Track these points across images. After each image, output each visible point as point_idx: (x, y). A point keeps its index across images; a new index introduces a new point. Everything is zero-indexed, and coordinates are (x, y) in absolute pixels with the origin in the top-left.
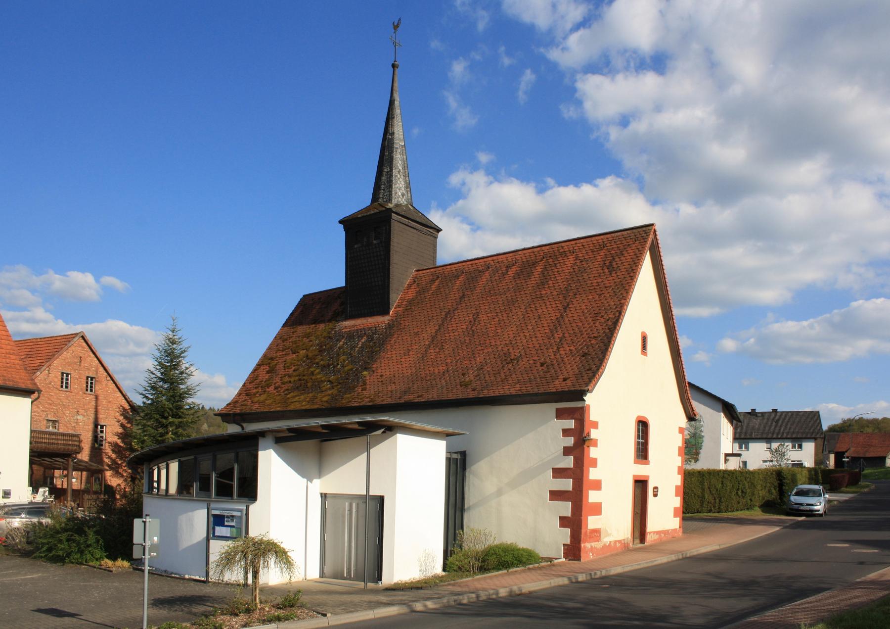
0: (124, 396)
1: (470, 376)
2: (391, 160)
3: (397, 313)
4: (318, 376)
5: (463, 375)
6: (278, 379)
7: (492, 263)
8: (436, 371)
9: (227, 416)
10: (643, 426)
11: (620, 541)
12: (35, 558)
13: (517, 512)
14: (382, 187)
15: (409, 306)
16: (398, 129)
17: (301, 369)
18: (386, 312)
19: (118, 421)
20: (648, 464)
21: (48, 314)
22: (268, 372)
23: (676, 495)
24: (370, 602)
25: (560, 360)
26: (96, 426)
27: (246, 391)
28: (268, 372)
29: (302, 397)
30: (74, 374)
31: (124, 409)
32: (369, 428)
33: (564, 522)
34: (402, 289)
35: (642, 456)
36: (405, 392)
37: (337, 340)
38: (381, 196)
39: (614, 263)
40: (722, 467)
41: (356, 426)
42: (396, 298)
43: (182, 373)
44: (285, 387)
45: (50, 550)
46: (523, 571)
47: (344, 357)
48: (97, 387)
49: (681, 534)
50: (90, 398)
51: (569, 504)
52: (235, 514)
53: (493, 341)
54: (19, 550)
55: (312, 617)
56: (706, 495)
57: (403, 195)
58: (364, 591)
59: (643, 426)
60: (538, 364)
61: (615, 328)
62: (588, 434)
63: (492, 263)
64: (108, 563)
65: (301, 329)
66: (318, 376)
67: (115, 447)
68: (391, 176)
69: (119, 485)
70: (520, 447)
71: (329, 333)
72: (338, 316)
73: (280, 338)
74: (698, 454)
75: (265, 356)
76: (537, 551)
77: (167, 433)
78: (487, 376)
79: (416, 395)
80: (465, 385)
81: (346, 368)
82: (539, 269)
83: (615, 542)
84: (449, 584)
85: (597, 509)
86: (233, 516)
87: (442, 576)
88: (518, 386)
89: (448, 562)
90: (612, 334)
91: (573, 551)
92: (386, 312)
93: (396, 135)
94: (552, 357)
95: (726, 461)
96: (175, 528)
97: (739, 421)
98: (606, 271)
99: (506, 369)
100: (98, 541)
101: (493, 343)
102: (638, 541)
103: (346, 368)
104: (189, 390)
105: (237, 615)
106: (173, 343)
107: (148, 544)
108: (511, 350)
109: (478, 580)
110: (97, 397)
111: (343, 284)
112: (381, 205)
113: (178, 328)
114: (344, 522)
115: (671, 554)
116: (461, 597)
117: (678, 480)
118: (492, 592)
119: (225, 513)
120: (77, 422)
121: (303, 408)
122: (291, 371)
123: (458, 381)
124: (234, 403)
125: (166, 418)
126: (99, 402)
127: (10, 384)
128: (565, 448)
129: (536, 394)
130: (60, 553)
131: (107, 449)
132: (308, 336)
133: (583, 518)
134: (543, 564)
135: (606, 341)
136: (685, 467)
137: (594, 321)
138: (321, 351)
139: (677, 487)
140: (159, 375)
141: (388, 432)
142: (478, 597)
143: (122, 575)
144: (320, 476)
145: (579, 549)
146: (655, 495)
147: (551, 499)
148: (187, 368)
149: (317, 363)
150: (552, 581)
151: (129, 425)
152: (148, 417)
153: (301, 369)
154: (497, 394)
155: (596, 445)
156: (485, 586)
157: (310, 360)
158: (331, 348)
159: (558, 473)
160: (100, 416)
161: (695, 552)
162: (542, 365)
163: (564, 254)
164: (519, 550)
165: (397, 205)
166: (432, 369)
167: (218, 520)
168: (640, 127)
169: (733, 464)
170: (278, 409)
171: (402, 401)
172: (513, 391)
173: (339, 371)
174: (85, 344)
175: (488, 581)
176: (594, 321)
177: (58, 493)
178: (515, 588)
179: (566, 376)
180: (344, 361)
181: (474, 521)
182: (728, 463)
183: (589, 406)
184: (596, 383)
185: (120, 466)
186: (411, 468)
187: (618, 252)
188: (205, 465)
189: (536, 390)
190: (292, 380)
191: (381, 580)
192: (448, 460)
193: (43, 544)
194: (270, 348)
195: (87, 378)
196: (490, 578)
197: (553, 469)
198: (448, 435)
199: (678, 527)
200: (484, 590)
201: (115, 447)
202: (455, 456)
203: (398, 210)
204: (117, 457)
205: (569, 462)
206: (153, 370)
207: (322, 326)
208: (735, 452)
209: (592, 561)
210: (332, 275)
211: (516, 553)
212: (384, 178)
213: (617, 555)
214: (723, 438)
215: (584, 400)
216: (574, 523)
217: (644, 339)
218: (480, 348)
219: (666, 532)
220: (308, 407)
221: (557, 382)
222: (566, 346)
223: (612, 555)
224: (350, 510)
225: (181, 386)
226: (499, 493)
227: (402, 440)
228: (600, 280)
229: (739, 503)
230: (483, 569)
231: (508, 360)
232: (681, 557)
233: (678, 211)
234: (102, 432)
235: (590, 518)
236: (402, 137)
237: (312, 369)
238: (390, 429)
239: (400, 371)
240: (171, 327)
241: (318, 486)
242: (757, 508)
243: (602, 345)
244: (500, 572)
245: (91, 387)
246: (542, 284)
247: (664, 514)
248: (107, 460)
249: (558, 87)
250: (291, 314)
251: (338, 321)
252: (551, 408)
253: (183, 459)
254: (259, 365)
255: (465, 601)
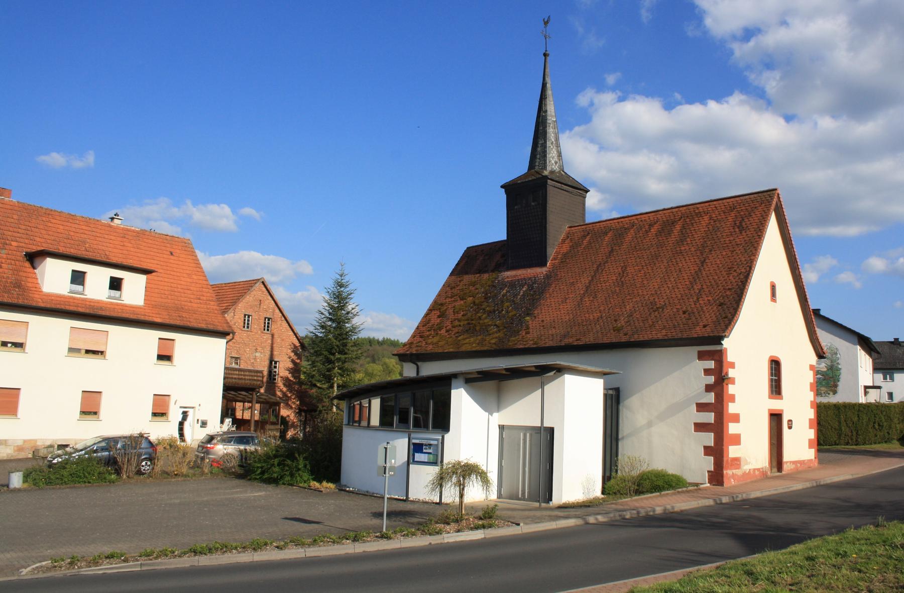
0: (295, 334)
1: (622, 322)
2: (545, 133)
3: (553, 265)
5: (616, 321)
6: (448, 323)
8: (591, 317)
10: (775, 365)
11: (758, 470)
13: (667, 442)
15: (565, 258)
16: (551, 108)
17: (469, 314)
19: (290, 358)
20: (782, 399)
21: (137, 225)
22: (439, 317)
23: (810, 428)
26: (271, 363)
27: (419, 333)
28: (439, 317)
30: (255, 316)
31: (295, 346)
32: (542, 370)
33: (708, 451)
34: (556, 243)
36: (565, 336)
40: (862, 400)
41: (533, 369)
43: (348, 313)
44: (455, 330)
45: (263, 473)
46: (674, 494)
47: (507, 304)
48: (273, 327)
49: (816, 464)
50: (267, 337)
51: (712, 435)
52: (432, 442)
54: (233, 473)
56: (839, 427)
57: (556, 163)
59: (775, 365)
61: (747, 281)
62: (727, 374)
63: (636, 221)
64: (316, 484)
65: (467, 278)
68: (545, 147)
70: (668, 385)
71: (493, 282)
72: (499, 268)
74: (836, 386)
75: (435, 302)
77: (334, 368)
79: (575, 339)
80: (617, 330)
82: (678, 227)
83: (754, 470)
91: (717, 477)
93: (549, 113)
95: (866, 393)
96: (377, 453)
97: (878, 353)
100: (305, 466)
101: (641, 293)
102: (775, 470)
105: (448, 524)
107: (388, 465)
110: (273, 336)
112: (537, 173)
113: (346, 272)
117: (811, 414)
119: (424, 442)
121: (474, 349)
122: (460, 316)
123: (611, 326)
124: (410, 344)
125: (334, 354)
127: (211, 327)
129: (681, 339)
130: (275, 475)
131: (280, 383)
132: (473, 284)
133: (724, 447)
134: (690, 488)
135: (739, 292)
139: (810, 420)
140: (328, 315)
142: (638, 513)
143: (330, 494)
145: (722, 476)
146: (790, 428)
151: (298, 361)
152: (317, 353)
153: (469, 314)
154: (646, 338)
155: (733, 383)
156: (642, 505)
157: (477, 306)
159: (701, 407)
160: (275, 353)
161: (828, 481)
162: (684, 313)
163: (699, 215)
164: (669, 475)
165: (552, 172)
166: (587, 315)
167: (417, 448)
168: (775, 38)
169: (873, 397)
170: (451, 350)
173: (504, 316)
177: (236, 421)
178: (669, 507)
179: (706, 323)
181: (627, 450)
182: (868, 395)
183: (726, 349)
185: (289, 398)
186: (576, 402)
188: (405, 400)
190: (462, 324)
192: (605, 396)
194: (439, 295)
197: (697, 404)
199: (813, 457)
202: (611, 392)
203: (553, 177)
205: (710, 398)
206: (323, 311)
207: (486, 276)
208: (876, 384)
209: (734, 486)
210: (494, 229)
212: (539, 149)
213: (755, 482)
216: (716, 451)
217: (773, 287)
219: (802, 462)
220: (478, 348)
221: (698, 328)
222: (704, 296)
224: (525, 440)
225: (347, 325)
226: (650, 424)
227: (570, 380)
230: (638, 492)
233: (816, 124)
234: (275, 367)
235: (731, 448)
238: (560, 370)
240: (340, 272)
241: (497, 419)
242: (895, 442)
243: (735, 296)
246: (681, 241)
247: (799, 445)
248: (279, 394)
251: (501, 272)
252: (694, 350)
254: (430, 310)
255: (628, 517)
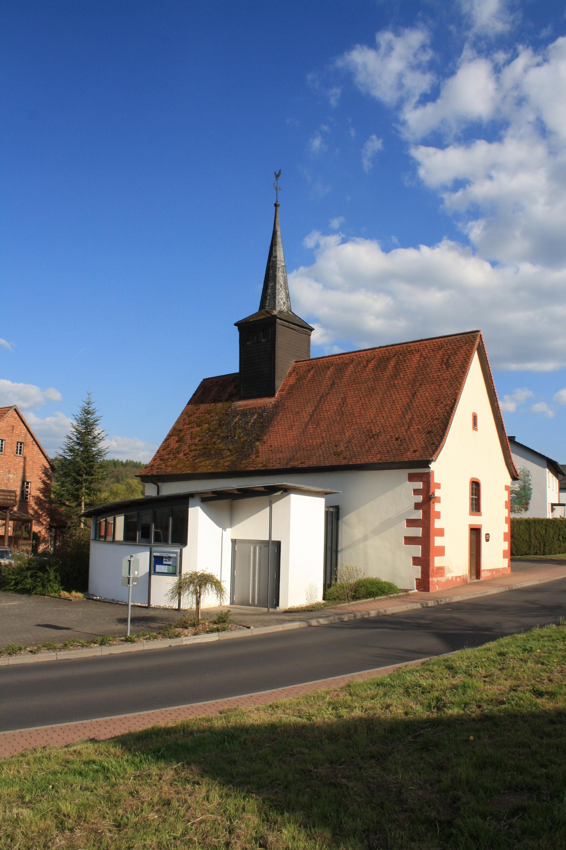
1: (342, 447)
2: (275, 277)
3: (281, 396)
4: (220, 446)
5: (336, 446)
7: (355, 357)
8: (315, 443)
9: (150, 476)
10: (476, 486)
11: (460, 577)
12: (4, 590)
13: (379, 555)
14: (268, 297)
15: (291, 390)
18: (272, 395)
19: (40, 479)
20: (480, 515)
22: (177, 442)
23: (505, 540)
24: (277, 620)
25: (410, 436)
26: (23, 482)
27: (160, 456)
28: (177, 442)
29: (207, 462)
30: (8, 441)
32: (270, 490)
34: (284, 376)
35: (476, 509)
36: (291, 460)
37: (234, 417)
38: (267, 304)
39: (450, 361)
42: (279, 384)
43: (94, 438)
44: (193, 454)
45: (16, 584)
46: (386, 599)
47: (240, 430)
48: (25, 451)
49: (509, 572)
50: (20, 459)
51: (420, 547)
52: (171, 555)
53: (358, 420)
55: (240, 629)
57: (284, 304)
58: (268, 613)
59: (476, 486)
60: (394, 439)
61: (452, 412)
62: (433, 493)
63: (355, 357)
64: (65, 594)
65: (203, 407)
66: (220, 446)
67: (38, 501)
68: (275, 289)
69: (40, 532)
71: (226, 410)
72: (232, 398)
73: (186, 413)
74: (527, 504)
76: (396, 584)
77: (82, 488)
78: (354, 447)
79: (300, 462)
80: (337, 454)
81: (242, 440)
82: (392, 363)
83: (456, 577)
84: (332, 608)
85: (441, 551)
86: (170, 557)
87: (323, 603)
88: (379, 456)
89: (327, 593)
90: (450, 417)
91: (423, 584)
92: (272, 394)
93: (278, 258)
94: (405, 433)
95: (553, 510)
96: (122, 566)
98: (444, 366)
99: (369, 442)
101: (358, 422)
102: (474, 577)
103: (242, 440)
104: (100, 452)
105: (186, 628)
106: (88, 413)
107: (132, 576)
108: (372, 428)
109: (353, 605)
111: (237, 370)
113: (92, 401)
114: (249, 561)
115: (500, 587)
116: (343, 616)
117: (506, 528)
118: (364, 613)
119: (164, 555)
120: (9, 479)
121: (209, 471)
123: (332, 451)
124: (151, 466)
125: (81, 476)
126: (27, 462)
128: (415, 503)
129: (393, 463)
130: (28, 586)
131: (32, 502)
132: (209, 412)
133: (430, 558)
134: (401, 594)
136: (517, 516)
137: (436, 406)
138: (220, 425)
141: (285, 493)
142: (355, 616)
144: (231, 526)
145: (428, 583)
146: (487, 540)
147: (405, 544)
148: (99, 434)
149: (218, 435)
150: (409, 606)
151: (49, 482)
153: (205, 440)
154: (363, 462)
155: (439, 502)
158: (229, 423)
159: (411, 523)
160: (27, 474)
161: (519, 586)
163: (411, 352)
164: (382, 583)
166: (310, 441)
170: (189, 472)
171: (289, 467)
172: (375, 460)
174: (17, 415)
175: (361, 606)
176: (436, 406)
178: (382, 610)
179: (415, 448)
180: (240, 434)
181: (346, 561)
183: (433, 472)
184: (438, 455)
185: (40, 516)
186: (300, 519)
187: (453, 352)
188: (147, 517)
189: (393, 460)
190: (198, 448)
191: (278, 605)
192: (327, 513)
193: (12, 579)
194: (178, 422)
195: (18, 442)
196: (362, 603)
198: (327, 493)
199: (506, 566)
200: (359, 611)
201: (37, 499)
202: (331, 510)
203: (282, 316)
204: (39, 508)
205: (419, 514)
206: (71, 436)
207: (220, 405)
209: (439, 592)
210: (230, 365)
211: (380, 585)
212: (269, 291)
213: (457, 587)
214: (549, 491)
215: (429, 467)
217: (475, 418)
218: (348, 425)
219: (497, 570)
220: (213, 470)
221: (409, 453)
223: (454, 588)
226: (366, 538)
227: (294, 498)
228: (439, 374)
229: (560, 547)
231: (371, 435)
232: (508, 589)
234: (27, 487)
235: (436, 558)
236: (283, 259)
237: (214, 440)
238: (286, 490)
239: (286, 443)
241: (230, 533)
243: (442, 425)
244: (369, 600)
245: (20, 450)
246: (395, 375)
247: (495, 555)
248: (31, 512)
249: (397, 158)
250: (194, 395)
251: (233, 401)
252: (405, 473)
253: (128, 514)
254: (170, 436)
255: (345, 619)
